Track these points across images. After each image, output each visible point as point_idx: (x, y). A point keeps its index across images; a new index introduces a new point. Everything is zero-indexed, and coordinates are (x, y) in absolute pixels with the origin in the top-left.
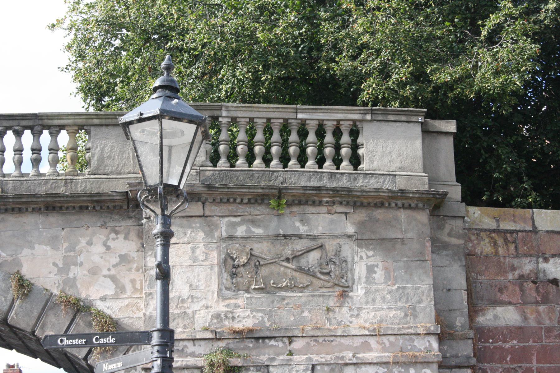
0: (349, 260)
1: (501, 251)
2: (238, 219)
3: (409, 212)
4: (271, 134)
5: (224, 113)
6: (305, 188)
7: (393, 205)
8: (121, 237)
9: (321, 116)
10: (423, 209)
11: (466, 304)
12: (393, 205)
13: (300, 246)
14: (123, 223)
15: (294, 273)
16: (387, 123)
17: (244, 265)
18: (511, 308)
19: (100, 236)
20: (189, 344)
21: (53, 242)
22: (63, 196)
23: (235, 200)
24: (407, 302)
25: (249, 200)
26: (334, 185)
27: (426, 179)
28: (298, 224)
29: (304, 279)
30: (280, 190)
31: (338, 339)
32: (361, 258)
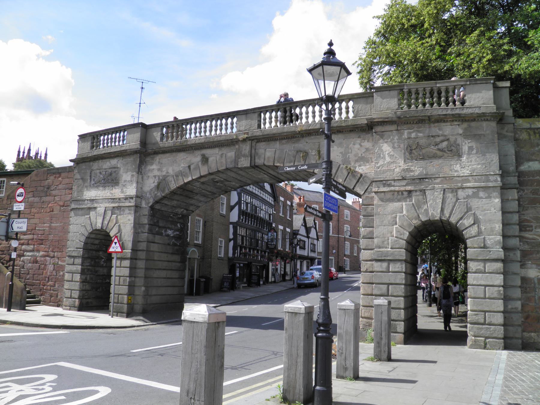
0: (460, 144)
1: (532, 137)
2: (412, 131)
3: (487, 122)
4: (404, 95)
5: (405, 87)
6: (439, 115)
7: (480, 120)
8: (366, 141)
9: (447, 84)
10: (494, 121)
11: (514, 161)
12: (480, 120)
13: (438, 140)
14: (367, 136)
15: (436, 151)
16: (477, 85)
17: (415, 149)
18: (537, 162)
19: (358, 141)
20: (392, 182)
21: (94, 211)
22: (343, 126)
23: (410, 122)
24: (486, 161)
25: (416, 122)
26: (453, 113)
27: (495, 107)
28: (437, 131)
29: (439, 153)
30: (429, 117)
31: (455, 178)
32: (466, 143)
